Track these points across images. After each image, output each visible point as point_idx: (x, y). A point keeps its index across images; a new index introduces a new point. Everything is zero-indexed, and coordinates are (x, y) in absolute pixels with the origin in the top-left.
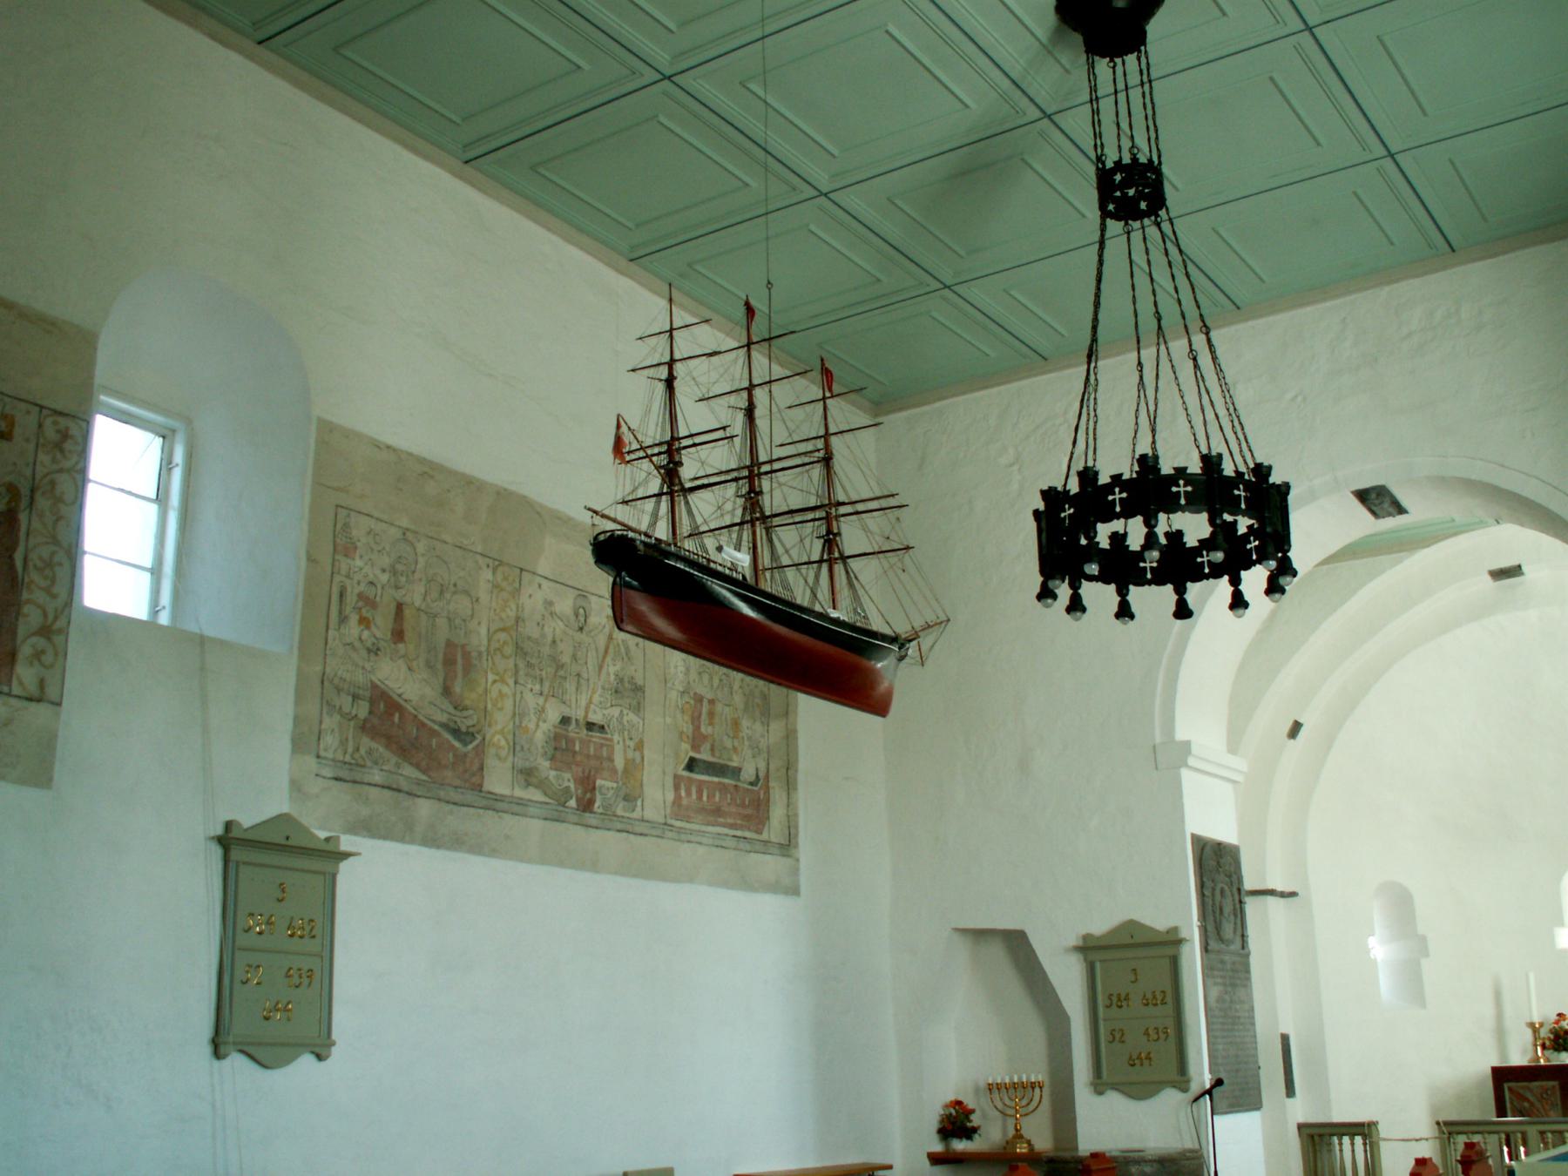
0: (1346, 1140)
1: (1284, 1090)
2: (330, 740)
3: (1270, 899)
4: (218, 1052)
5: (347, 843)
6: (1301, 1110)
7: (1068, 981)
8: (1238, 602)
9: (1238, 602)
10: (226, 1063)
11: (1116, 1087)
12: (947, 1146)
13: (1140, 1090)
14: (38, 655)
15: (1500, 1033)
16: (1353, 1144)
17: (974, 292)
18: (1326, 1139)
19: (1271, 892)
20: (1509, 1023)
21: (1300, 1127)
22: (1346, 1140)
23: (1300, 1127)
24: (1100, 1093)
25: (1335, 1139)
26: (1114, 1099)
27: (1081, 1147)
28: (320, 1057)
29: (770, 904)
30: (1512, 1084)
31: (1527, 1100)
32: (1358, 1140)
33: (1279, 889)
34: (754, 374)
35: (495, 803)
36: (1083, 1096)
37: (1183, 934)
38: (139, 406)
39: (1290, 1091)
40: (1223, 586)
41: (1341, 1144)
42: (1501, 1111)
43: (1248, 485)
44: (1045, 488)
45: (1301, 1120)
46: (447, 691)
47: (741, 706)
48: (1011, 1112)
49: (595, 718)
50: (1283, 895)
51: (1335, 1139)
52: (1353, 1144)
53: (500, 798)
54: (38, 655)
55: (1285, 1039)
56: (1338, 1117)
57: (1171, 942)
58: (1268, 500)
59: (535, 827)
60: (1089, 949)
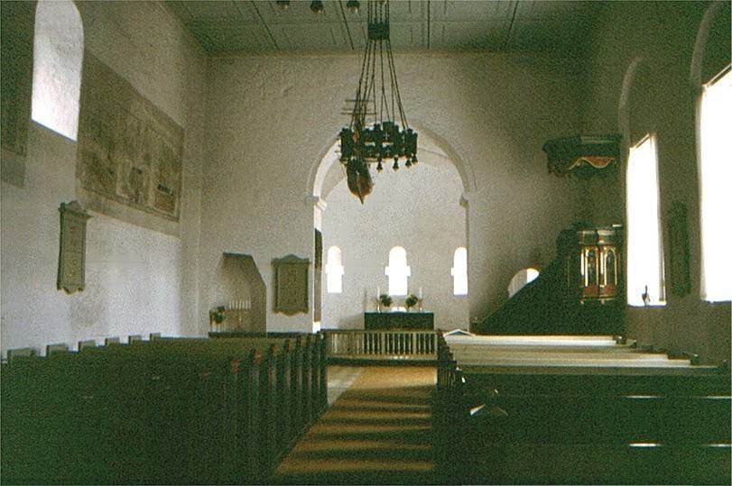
2: (84, 174)
4: (59, 288)
5: (90, 212)
7: (267, 274)
8: (396, 167)
9: (396, 167)
10: (60, 291)
12: (408, 310)
14: (21, 138)
15: (365, 302)
20: (369, 298)
28: (80, 289)
29: (172, 239)
32: (346, 336)
35: (118, 198)
37: (310, 261)
40: (392, 161)
43: (406, 136)
46: (109, 157)
49: (140, 168)
53: (118, 197)
54: (21, 138)
57: (276, 310)
58: (411, 138)
59: (125, 208)
60: (276, 264)
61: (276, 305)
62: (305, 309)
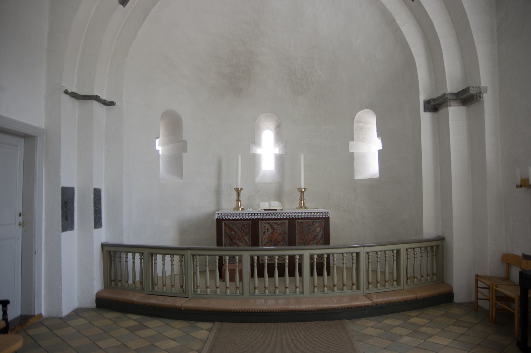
0: (130, 255)
3: (95, 103)
6: (102, 236)
17: (412, 331)
19: (97, 98)
21: (103, 246)
22: (168, 258)
23: (103, 246)
25: (123, 255)
27: (424, 234)
30: (250, 224)
31: (233, 230)
32: (137, 256)
33: (103, 97)
39: (98, 223)
42: (219, 243)
44: (121, 6)
45: (104, 240)
47: (480, 303)
50: (106, 103)
51: (130, 255)
55: (97, 193)
56: (127, 240)
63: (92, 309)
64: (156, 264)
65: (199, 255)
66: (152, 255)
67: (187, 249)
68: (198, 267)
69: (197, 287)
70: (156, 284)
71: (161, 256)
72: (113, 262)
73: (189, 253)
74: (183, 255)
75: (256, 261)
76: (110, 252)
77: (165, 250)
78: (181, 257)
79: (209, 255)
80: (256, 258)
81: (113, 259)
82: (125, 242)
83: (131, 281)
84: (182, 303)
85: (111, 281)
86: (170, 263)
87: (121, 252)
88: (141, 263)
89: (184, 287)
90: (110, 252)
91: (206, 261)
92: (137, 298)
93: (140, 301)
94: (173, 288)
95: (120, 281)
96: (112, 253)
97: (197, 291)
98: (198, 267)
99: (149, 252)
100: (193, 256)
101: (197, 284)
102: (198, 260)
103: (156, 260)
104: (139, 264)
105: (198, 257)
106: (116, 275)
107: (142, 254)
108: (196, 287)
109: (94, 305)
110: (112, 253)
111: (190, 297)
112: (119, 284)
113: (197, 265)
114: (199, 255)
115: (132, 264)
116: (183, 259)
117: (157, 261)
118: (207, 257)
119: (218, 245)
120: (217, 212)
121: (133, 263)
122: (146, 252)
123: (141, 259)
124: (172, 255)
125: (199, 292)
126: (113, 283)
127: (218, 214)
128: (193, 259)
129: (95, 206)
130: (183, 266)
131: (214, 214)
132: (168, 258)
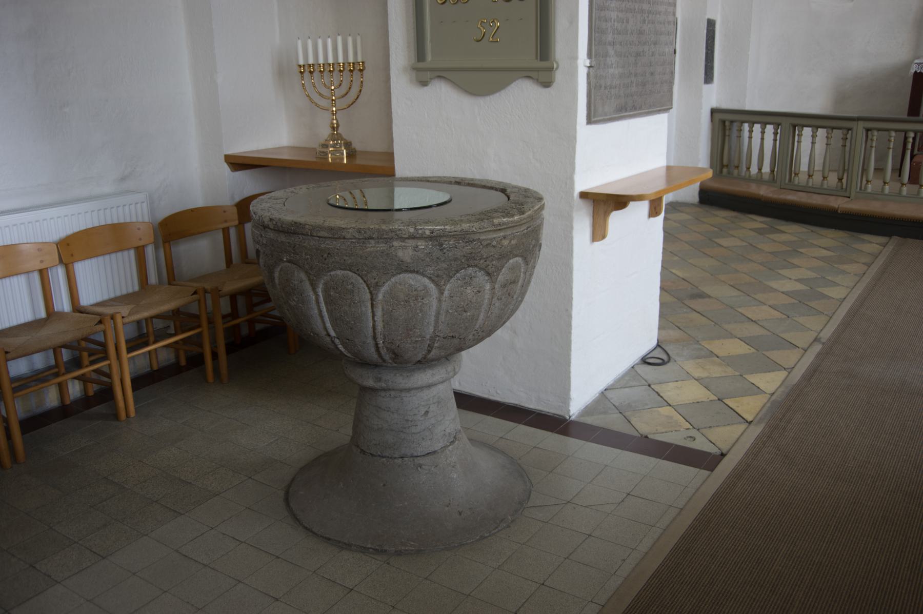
1: (703, 76)
6: (714, 96)
11: (442, 74)
13: (480, 80)
16: (763, 133)
18: (736, 125)
21: (713, 111)
22: (757, 128)
23: (713, 111)
24: (424, 83)
26: (442, 91)
32: (770, 129)
34: (742, 431)
36: (402, 86)
38: (328, 311)
39: (709, 77)
41: (751, 131)
45: (715, 105)
48: (324, 103)
51: (746, 126)
52: (763, 133)
55: (711, 24)
57: (424, 72)
61: (420, 55)
62: (541, 66)
63: (693, 205)
64: (799, 142)
65: (879, 130)
66: (794, 127)
67: (859, 119)
68: (873, 149)
69: (868, 181)
70: (796, 174)
71: (810, 129)
72: (727, 138)
73: (861, 125)
74: (849, 129)
75: (911, 140)
76: (724, 122)
77: (814, 120)
78: (845, 132)
79: (896, 131)
80: (912, 135)
81: (727, 133)
82: (748, 107)
83: (754, 170)
84: (838, 203)
85: (722, 166)
86: (760, 135)
87: (743, 122)
88: (775, 140)
89: (844, 181)
90: (724, 122)
91: (890, 141)
92: (764, 192)
93: (770, 195)
94: (825, 182)
95: (737, 167)
96: (727, 123)
97: (866, 188)
98: (873, 149)
99: (789, 123)
100: (868, 130)
101: (867, 177)
102: (875, 138)
103: (800, 135)
104: (772, 142)
105: (875, 133)
106: (729, 160)
107: (777, 125)
108: (864, 182)
109: (695, 199)
110: (726, 124)
111: (852, 196)
112: (736, 172)
113: (872, 147)
114: (879, 130)
115: (759, 141)
116: (849, 136)
117: (803, 138)
118: (893, 134)
119: (910, 114)
120: (916, 61)
121: (760, 143)
122: (786, 122)
123: (775, 134)
124: (764, 125)
125: (869, 190)
126: (725, 170)
127: (918, 64)
128: (867, 136)
129: (707, 48)
130: (847, 148)
131: (908, 65)
132: (757, 128)
